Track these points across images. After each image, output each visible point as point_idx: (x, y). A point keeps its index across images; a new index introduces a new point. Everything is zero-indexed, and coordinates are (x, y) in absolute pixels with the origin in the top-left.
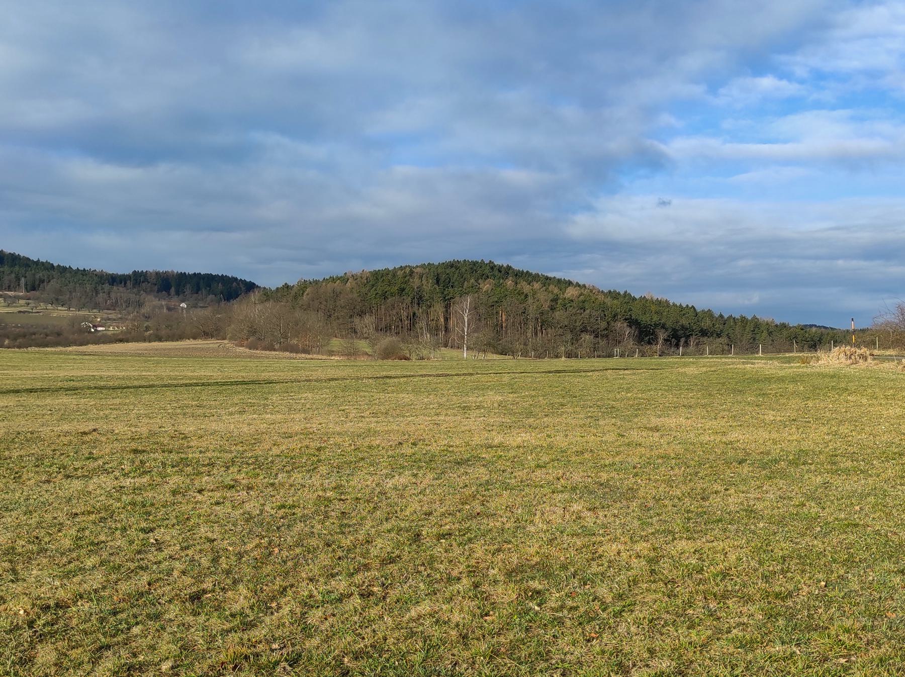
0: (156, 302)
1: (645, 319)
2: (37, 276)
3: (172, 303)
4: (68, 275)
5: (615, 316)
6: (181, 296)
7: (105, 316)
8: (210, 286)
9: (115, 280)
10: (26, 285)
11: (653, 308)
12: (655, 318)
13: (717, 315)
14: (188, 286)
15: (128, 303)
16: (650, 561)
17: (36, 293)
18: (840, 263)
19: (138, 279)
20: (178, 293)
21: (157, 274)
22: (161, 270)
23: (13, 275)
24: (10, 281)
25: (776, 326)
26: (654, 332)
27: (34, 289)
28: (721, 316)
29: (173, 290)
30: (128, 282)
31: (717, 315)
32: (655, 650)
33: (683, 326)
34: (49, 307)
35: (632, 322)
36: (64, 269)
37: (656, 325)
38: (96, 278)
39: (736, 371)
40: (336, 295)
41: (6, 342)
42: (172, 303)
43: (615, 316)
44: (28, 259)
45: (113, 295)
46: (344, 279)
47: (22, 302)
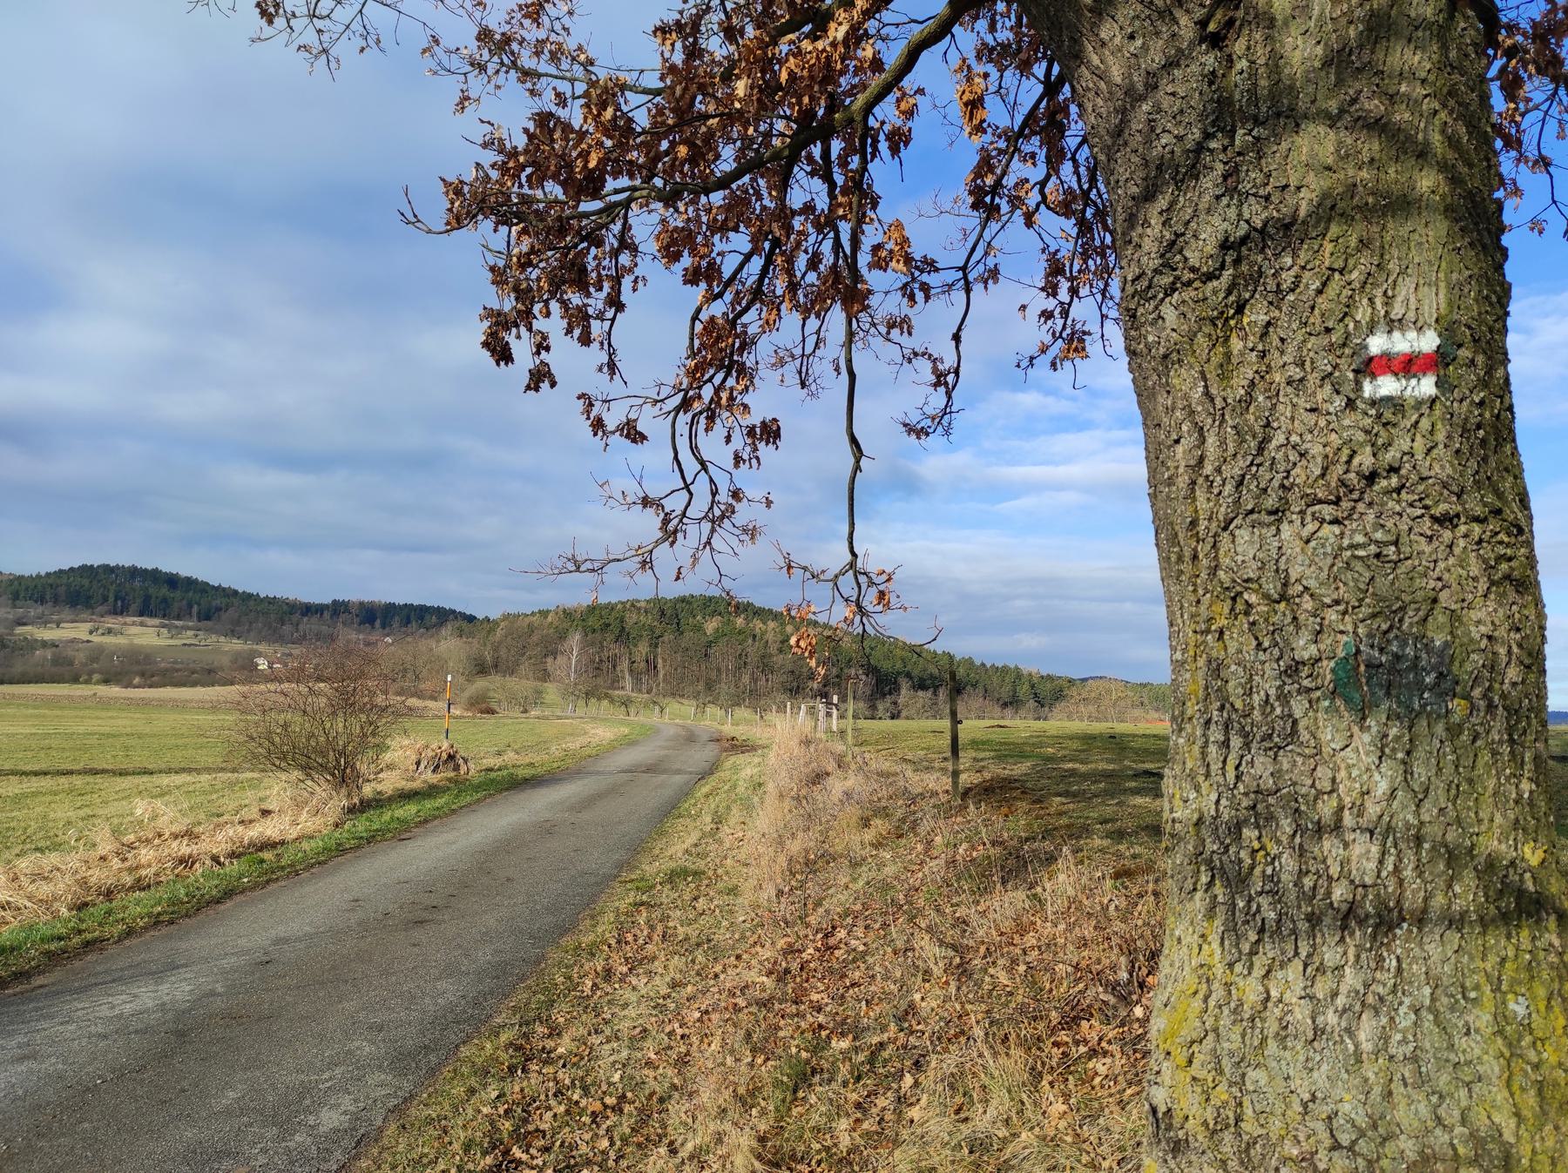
0: (353, 636)
1: (886, 666)
2: (214, 603)
3: (373, 638)
4: (252, 603)
5: (850, 661)
6: (387, 630)
7: (287, 651)
8: (422, 619)
9: (308, 610)
10: (199, 613)
11: (898, 652)
12: (899, 665)
13: (978, 663)
14: (397, 618)
15: (318, 636)
16: (1015, 920)
17: (209, 623)
18: (1128, 606)
19: (338, 609)
20: (383, 627)
21: (361, 604)
22: (366, 598)
23: (184, 602)
24: (180, 609)
25: (1042, 677)
26: (895, 683)
27: (208, 618)
28: (983, 665)
29: (378, 623)
30: (325, 613)
31: (978, 663)
32: (558, 1024)
33: (931, 675)
34: (222, 639)
35: (871, 670)
36: (250, 595)
37: (899, 673)
38: (285, 607)
39: (219, 724)
40: (531, 629)
41: (137, 680)
42: (373, 638)
43: (850, 661)
44: (207, 584)
45: (301, 627)
46: (544, 614)
47: (190, 633)
